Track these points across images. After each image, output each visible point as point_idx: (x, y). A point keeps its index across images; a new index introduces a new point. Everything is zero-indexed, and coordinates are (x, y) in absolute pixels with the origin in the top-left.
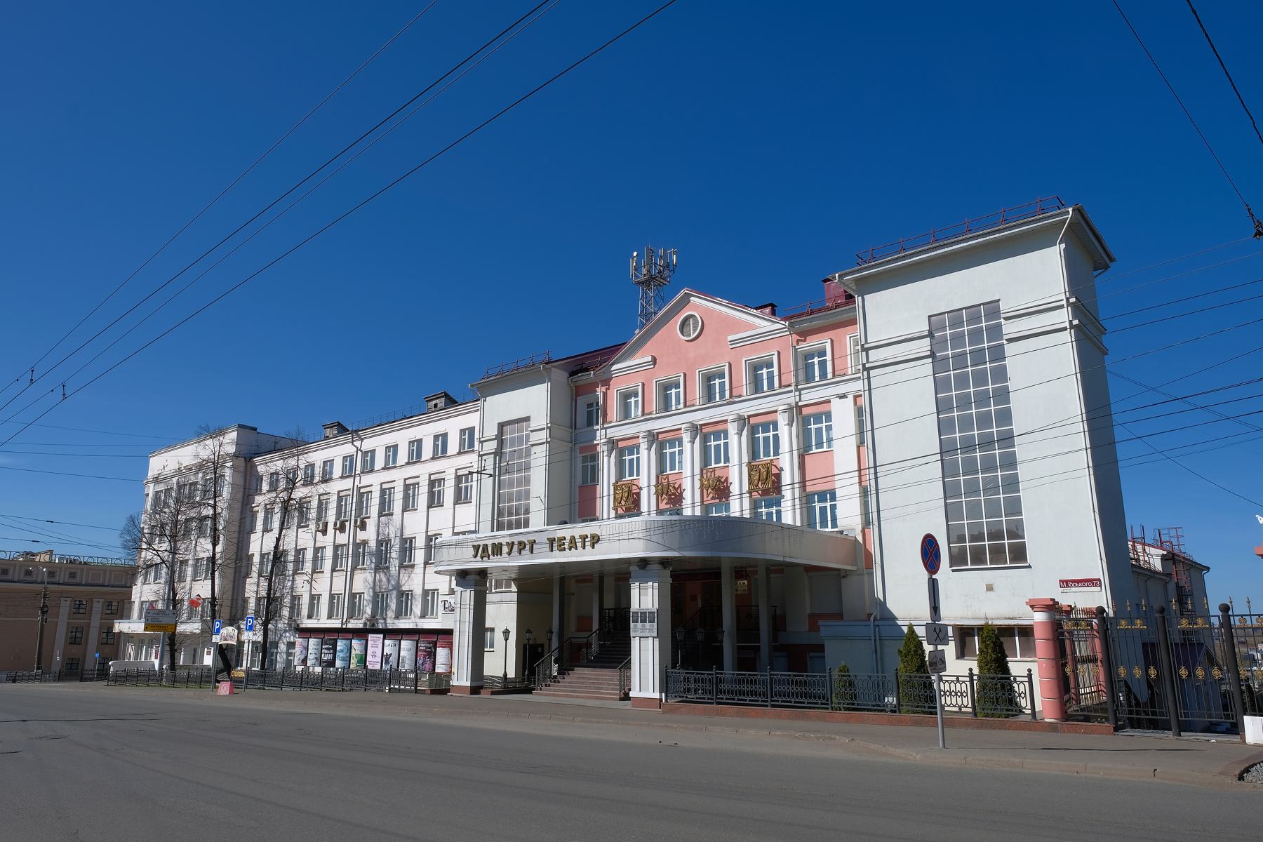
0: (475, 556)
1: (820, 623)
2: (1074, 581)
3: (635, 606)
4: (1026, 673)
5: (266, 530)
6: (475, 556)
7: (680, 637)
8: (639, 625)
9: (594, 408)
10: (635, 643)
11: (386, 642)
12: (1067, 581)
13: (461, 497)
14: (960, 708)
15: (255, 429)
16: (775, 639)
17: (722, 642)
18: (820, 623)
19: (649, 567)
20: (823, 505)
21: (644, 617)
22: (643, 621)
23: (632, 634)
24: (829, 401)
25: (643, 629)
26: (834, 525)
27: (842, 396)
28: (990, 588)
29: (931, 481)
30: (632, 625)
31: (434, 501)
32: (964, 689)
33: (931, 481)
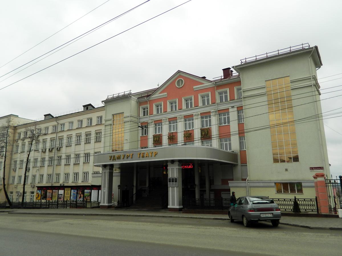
0: (110, 160)
1: (229, 182)
2: (314, 168)
3: (170, 176)
4: (315, 198)
5: (23, 152)
6: (110, 160)
7: (183, 187)
8: (171, 183)
9: (146, 110)
10: (170, 190)
11: (72, 191)
12: (312, 168)
13: (98, 140)
14: (312, 210)
15: (18, 116)
16: (210, 187)
17: (195, 188)
18: (229, 182)
19: (175, 163)
20: (226, 143)
21: (174, 180)
22: (173, 181)
23: (169, 186)
24: (229, 109)
25: (173, 185)
26: (230, 149)
27: (233, 107)
28: (286, 170)
29: (26, 187)
30: (168, 183)
31: (88, 142)
32: (314, 203)
33: (26, 187)
